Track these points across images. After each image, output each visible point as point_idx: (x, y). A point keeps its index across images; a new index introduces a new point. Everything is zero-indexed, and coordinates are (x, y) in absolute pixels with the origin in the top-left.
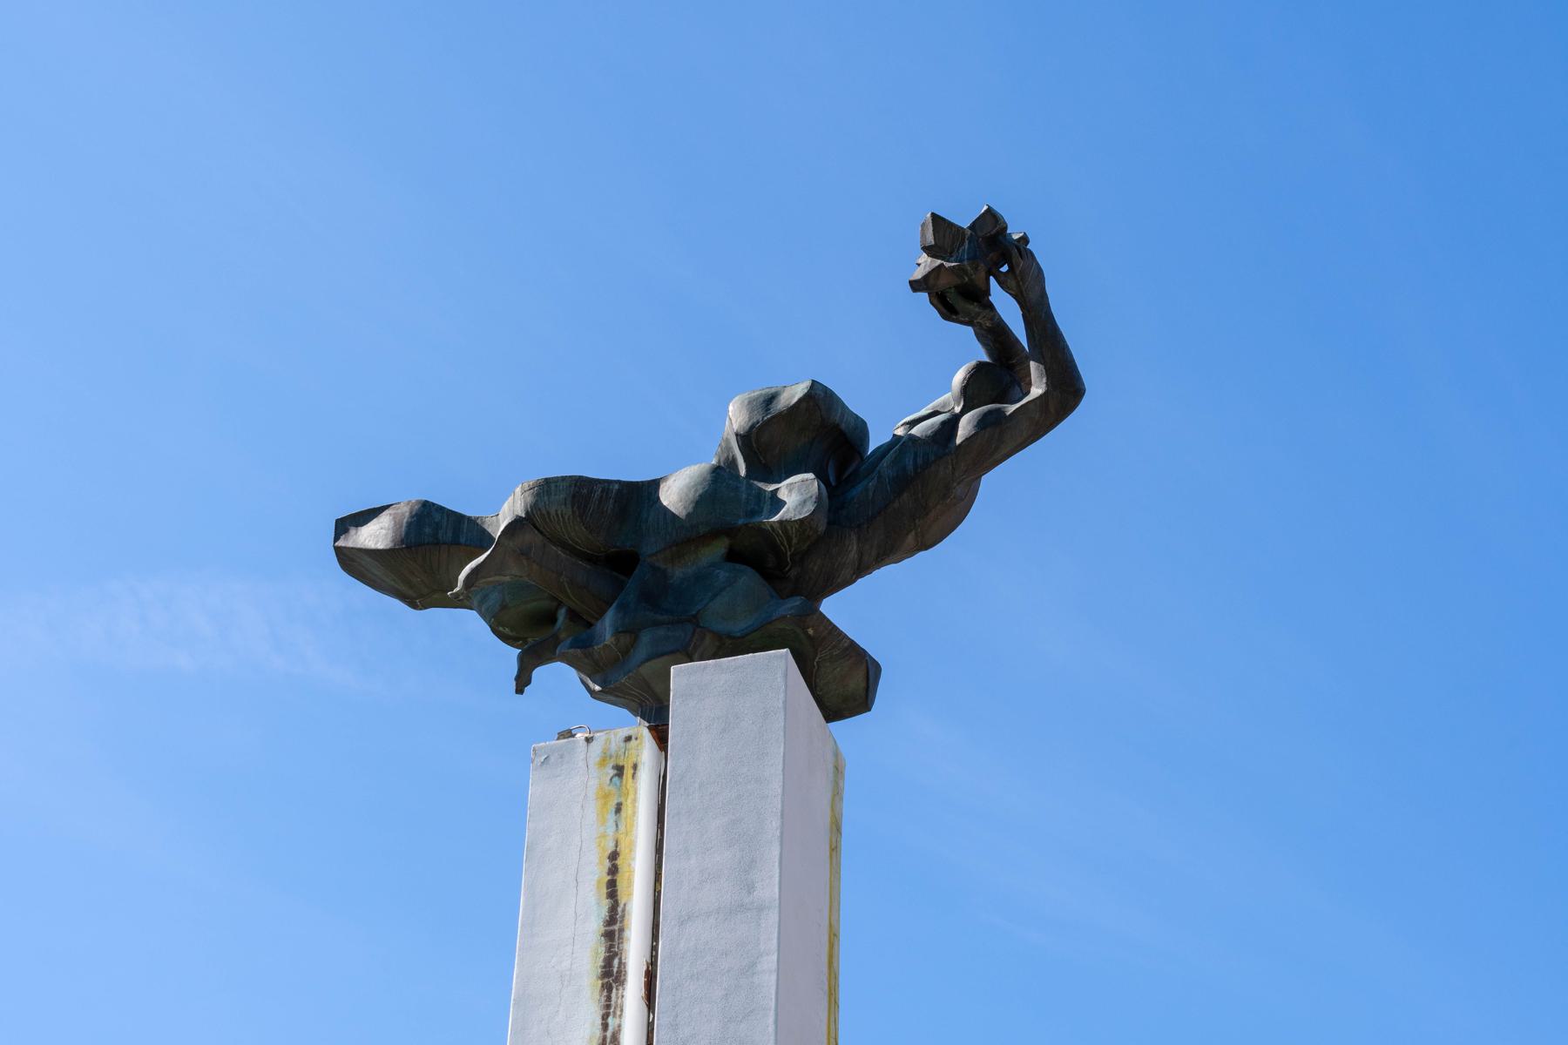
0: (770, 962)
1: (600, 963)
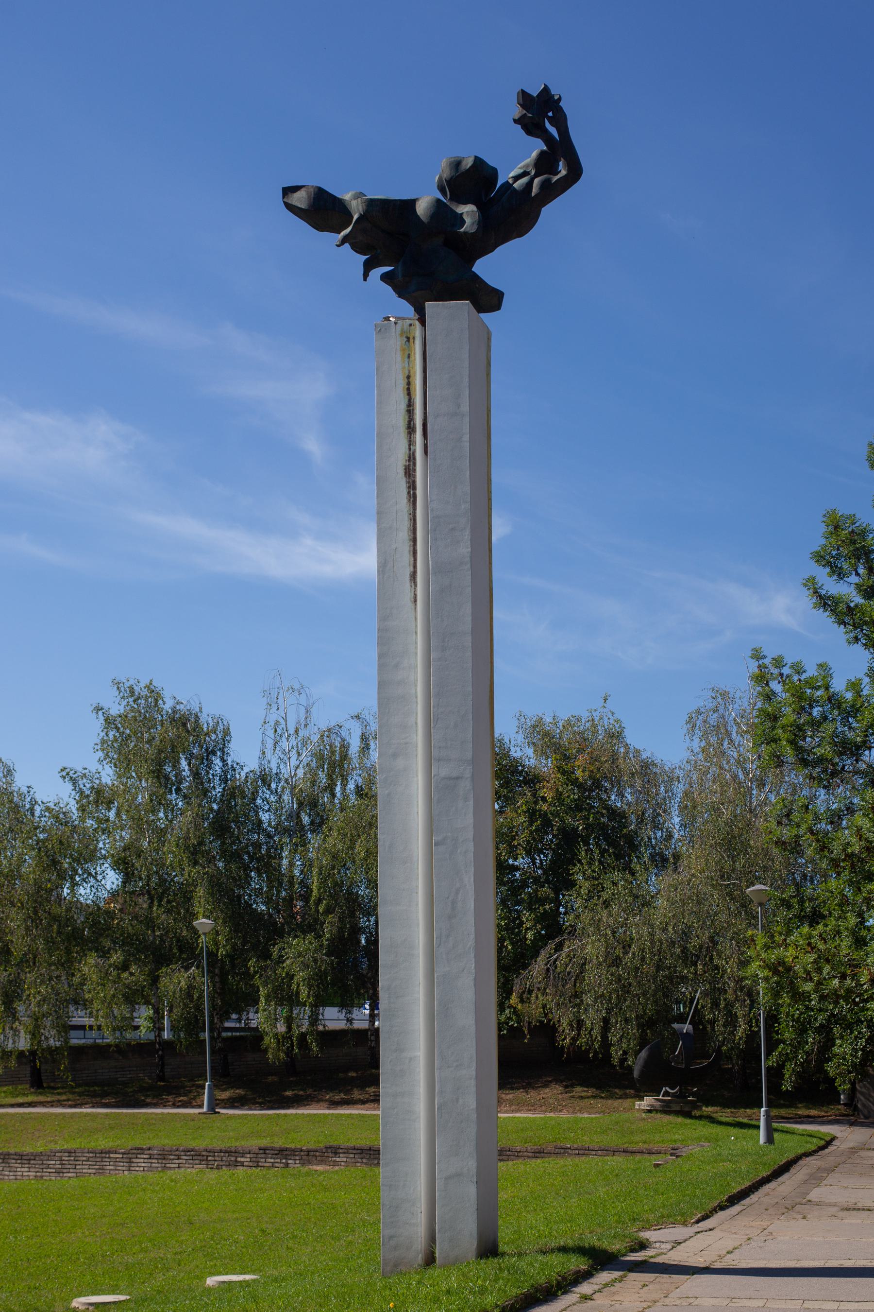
0: (466, 438)
1: (407, 423)
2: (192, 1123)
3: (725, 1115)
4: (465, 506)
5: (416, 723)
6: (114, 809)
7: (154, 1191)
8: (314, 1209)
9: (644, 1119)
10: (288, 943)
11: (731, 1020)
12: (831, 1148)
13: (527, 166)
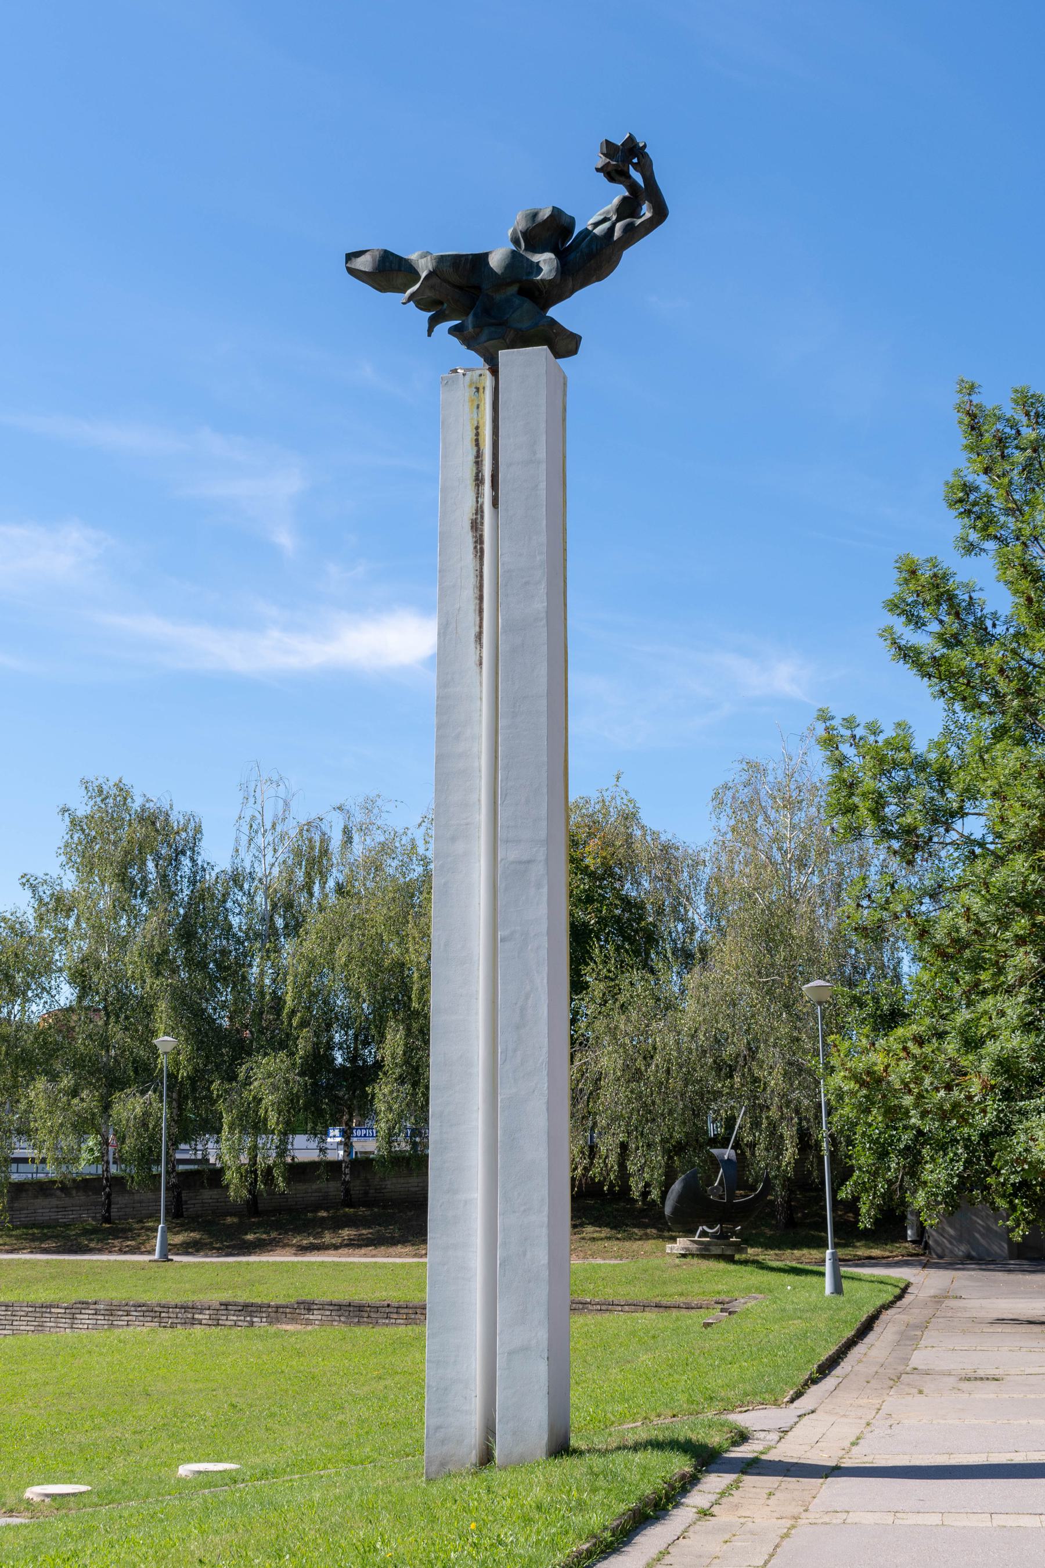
0: (543, 485)
1: (474, 475)
2: (142, 1272)
3: (769, 1257)
4: (541, 558)
5: (479, 800)
6: (74, 917)
7: (101, 1354)
8: (290, 1379)
9: (678, 1266)
10: (256, 1062)
11: (776, 1144)
12: (908, 1299)
13: (608, 212)
